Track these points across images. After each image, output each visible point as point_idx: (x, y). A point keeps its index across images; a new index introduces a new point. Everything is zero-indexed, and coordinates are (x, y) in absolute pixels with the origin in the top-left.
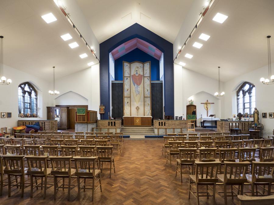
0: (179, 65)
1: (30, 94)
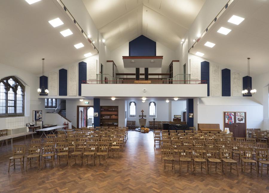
0: (196, 55)
1: (15, 90)
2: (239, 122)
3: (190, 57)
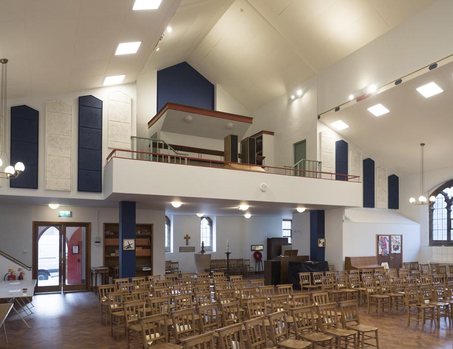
2: (395, 252)
3: (321, 129)
